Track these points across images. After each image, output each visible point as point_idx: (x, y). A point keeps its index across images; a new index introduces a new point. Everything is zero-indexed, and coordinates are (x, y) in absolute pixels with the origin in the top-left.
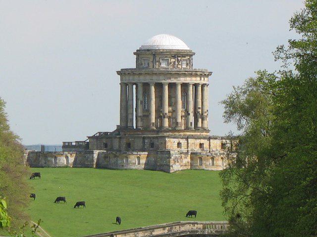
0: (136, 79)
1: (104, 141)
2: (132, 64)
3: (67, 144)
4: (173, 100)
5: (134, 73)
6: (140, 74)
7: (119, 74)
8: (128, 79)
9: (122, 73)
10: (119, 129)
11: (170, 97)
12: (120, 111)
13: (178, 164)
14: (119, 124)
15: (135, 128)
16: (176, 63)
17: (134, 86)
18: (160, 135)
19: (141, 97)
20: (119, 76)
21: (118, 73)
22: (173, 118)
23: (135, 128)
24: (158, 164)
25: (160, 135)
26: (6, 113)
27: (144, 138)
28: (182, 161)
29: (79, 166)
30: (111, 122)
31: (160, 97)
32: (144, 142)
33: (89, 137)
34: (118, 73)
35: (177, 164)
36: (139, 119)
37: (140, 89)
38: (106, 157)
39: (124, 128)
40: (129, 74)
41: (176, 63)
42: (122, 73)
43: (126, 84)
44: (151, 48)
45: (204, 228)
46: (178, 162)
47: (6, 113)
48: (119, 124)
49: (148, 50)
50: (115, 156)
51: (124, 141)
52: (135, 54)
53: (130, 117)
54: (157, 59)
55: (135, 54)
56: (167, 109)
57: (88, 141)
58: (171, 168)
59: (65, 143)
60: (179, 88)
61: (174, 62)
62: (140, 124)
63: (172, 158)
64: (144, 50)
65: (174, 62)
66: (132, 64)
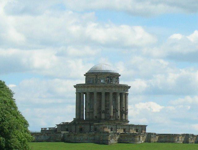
0: (86, 90)
3: (43, 129)
5: (84, 87)
6: (88, 87)
7: (75, 87)
8: (81, 90)
9: (77, 86)
10: (75, 120)
12: (163, 134)
13: (113, 139)
14: (75, 118)
15: (85, 119)
16: (110, 81)
17: (84, 95)
20: (75, 89)
21: (75, 86)
22: (107, 111)
23: (85, 119)
24: (101, 139)
26: (15, 100)
28: (115, 138)
29: (53, 141)
33: (57, 125)
34: (75, 86)
35: (112, 139)
36: (87, 113)
37: (88, 96)
38: (69, 136)
40: (81, 87)
41: (110, 81)
42: (77, 86)
43: (80, 94)
44: (95, 72)
46: (113, 138)
47: (15, 100)
48: (75, 118)
49: (93, 73)
50: (75, 135)
51: (78, 127)
52: (85, 75)
53: (82, 113)
54: (98, 78)
55: (85, 75)
56: (103, 108)
57: (56, 127)
58: (109, 142)
59: (42, 128)
61: (108, 80)
62: (88, 117)
63: (110, 135)
64: (91, 73)
65: (108, 80)
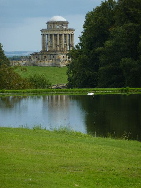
21: (41, 30)
27: (51, 55)
30: (38, 48)
31: (56, 39)
32: (42, 56)
39: (42, 51)
42: (42, 30)
51: (44, 56)
56: (58, 44)
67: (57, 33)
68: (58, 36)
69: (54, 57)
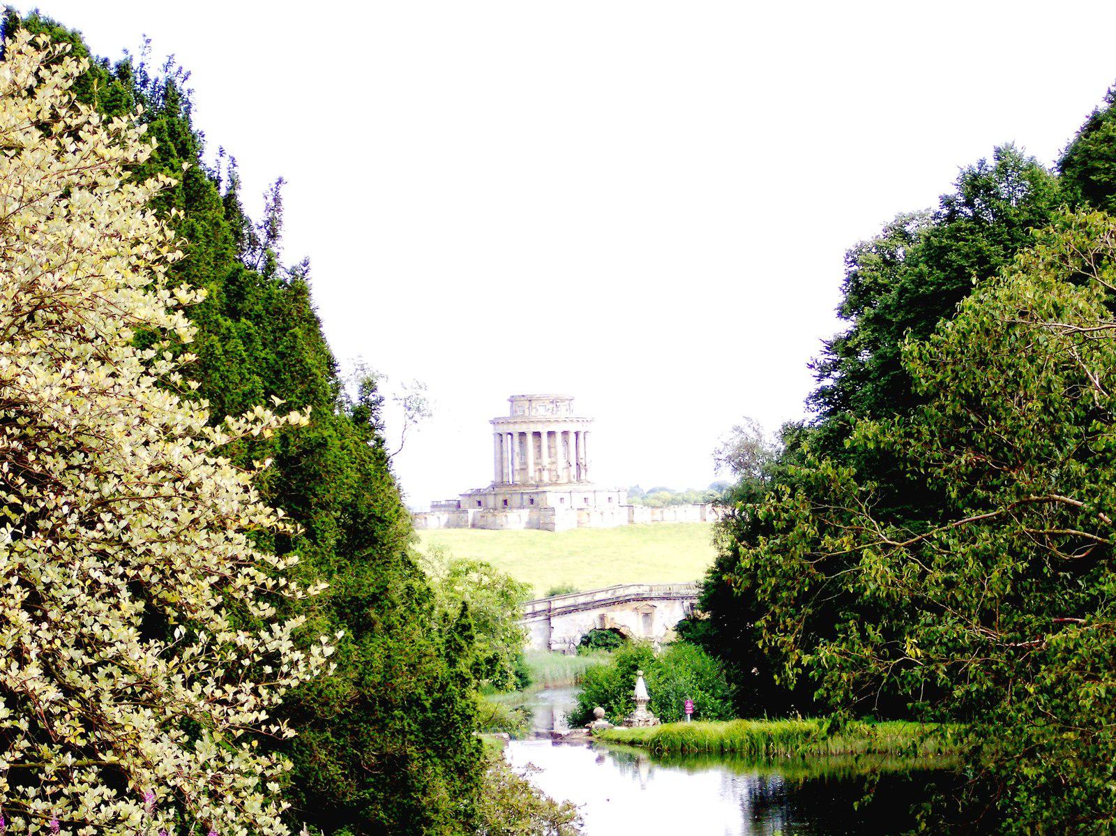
0: (511, 428)
1: (478, 498)
2: (504, 411)
4: (553, 450)
11: (549, 447)
18: (540, 489)
19: (517, 448)
25: (540, 489)
34: (493, 422)
42: (494, 422)
45: (651, 590)
53: (505, 471)
60: (530, 438)
66: (504, 411)
67: (538, 428)
68: (544, 437)
69: (532, 501)
